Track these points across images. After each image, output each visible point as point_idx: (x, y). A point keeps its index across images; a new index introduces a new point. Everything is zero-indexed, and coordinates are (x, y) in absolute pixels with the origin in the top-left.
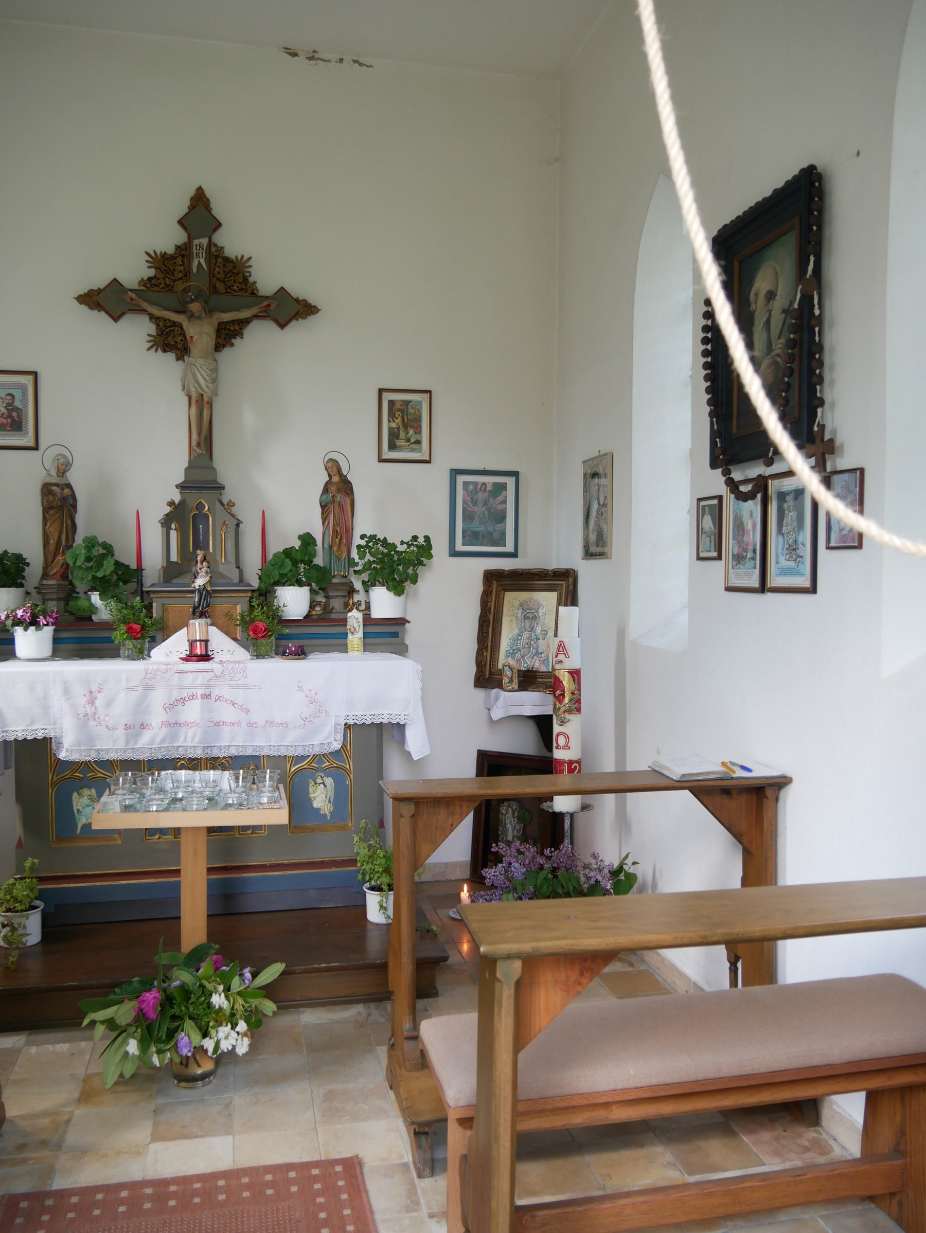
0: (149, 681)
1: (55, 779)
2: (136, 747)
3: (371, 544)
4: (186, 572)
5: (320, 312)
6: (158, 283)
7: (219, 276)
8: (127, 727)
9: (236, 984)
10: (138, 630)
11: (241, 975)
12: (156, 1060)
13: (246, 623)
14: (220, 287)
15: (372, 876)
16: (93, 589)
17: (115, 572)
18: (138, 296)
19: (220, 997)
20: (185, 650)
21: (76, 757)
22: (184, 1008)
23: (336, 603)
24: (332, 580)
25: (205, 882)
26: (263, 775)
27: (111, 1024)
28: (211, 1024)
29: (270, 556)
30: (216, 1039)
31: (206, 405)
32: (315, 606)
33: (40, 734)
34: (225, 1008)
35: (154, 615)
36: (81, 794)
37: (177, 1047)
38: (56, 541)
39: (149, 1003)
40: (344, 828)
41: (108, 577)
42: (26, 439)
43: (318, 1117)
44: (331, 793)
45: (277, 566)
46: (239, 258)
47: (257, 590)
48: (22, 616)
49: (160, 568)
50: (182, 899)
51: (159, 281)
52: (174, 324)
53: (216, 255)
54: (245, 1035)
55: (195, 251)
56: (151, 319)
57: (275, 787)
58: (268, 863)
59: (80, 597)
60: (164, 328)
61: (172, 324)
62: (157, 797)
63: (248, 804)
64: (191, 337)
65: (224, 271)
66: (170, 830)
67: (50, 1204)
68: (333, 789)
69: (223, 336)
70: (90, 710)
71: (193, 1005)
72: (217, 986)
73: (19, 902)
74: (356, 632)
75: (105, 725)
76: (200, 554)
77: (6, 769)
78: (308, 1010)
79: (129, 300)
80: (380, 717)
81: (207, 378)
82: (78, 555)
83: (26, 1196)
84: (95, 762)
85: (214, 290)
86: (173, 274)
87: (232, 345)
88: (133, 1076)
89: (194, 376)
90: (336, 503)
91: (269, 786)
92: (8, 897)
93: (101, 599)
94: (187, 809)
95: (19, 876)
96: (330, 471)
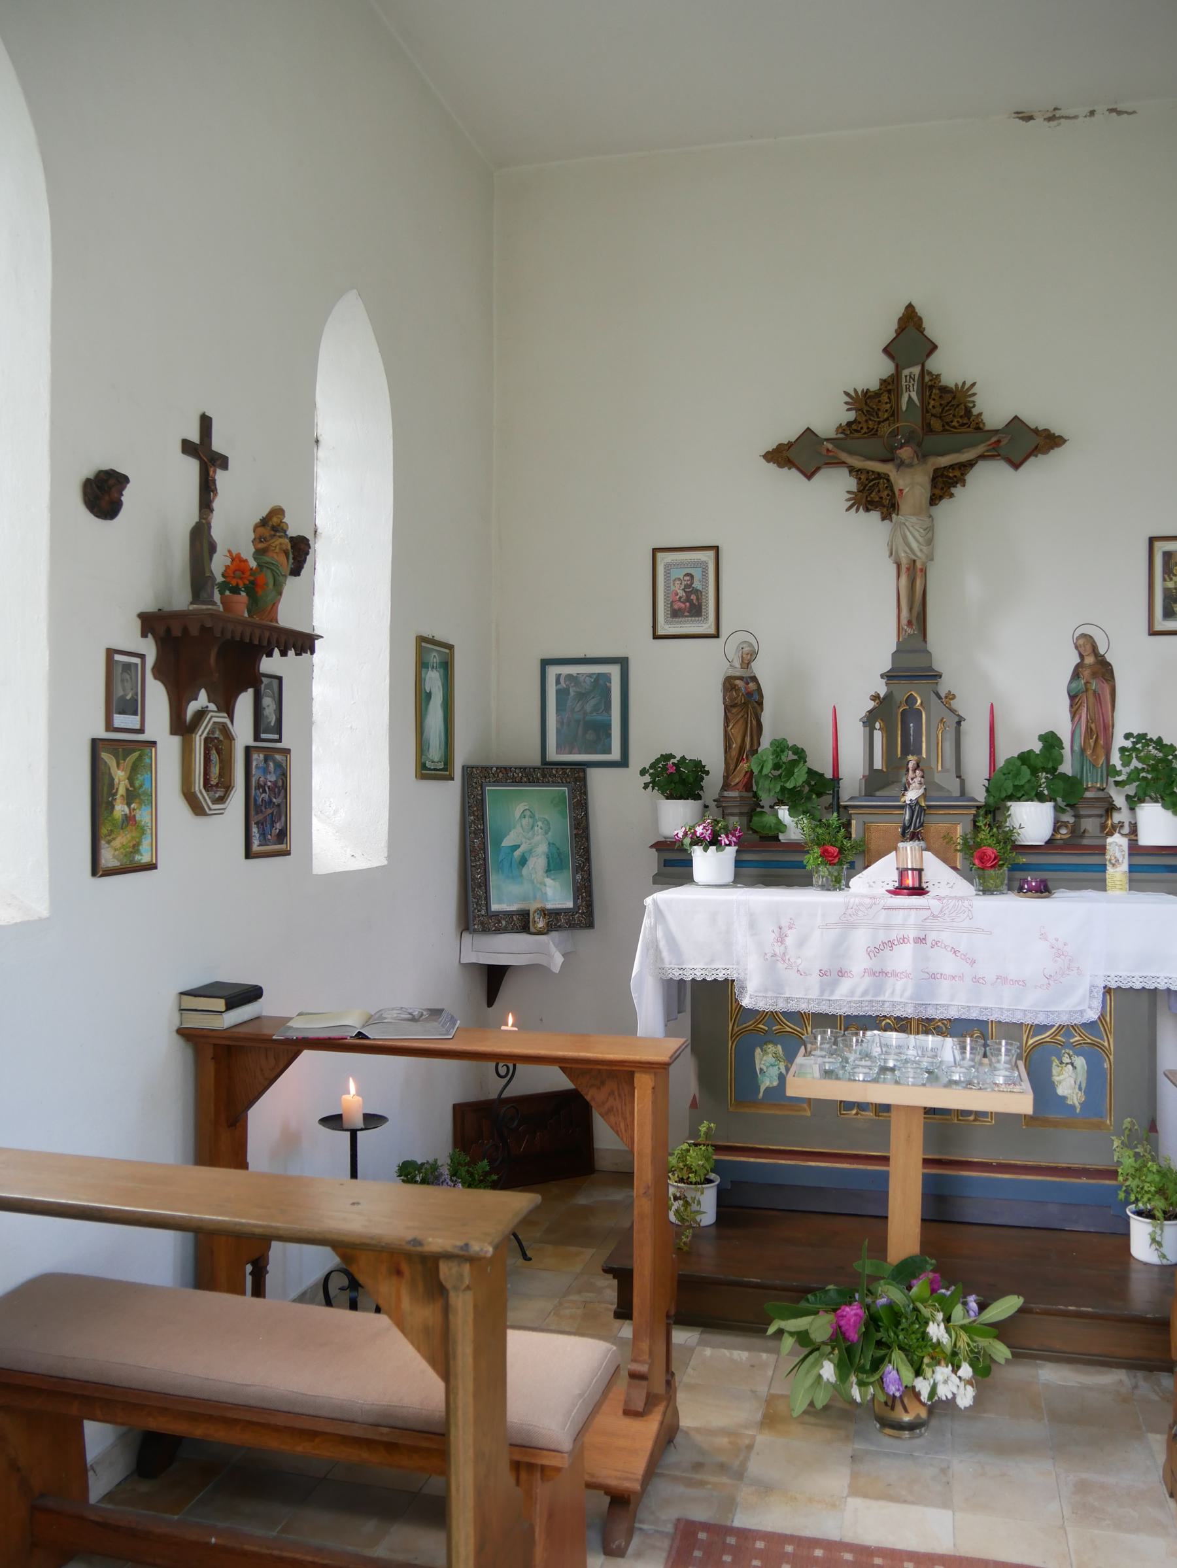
0: (850, 918)
1: (736, 1029)
2: (833, 998)
3: (1139, 746)
4: (893, 782)
5: (1067, 443)
6: (859, 429)
7: (934, 411)
8: (823, 973)
9: (958, 1312)
10: (835, 854)
11: (965, 1304)
12: (856, 1393)
13: (970, 848)
14: (936, 424)
15: (1139, 1196)
16: (781, 802)
17: (807, 782)
18: (836, 446)
19: (939, 1328)
20: (892, 880)
21: (761, 1005)
22: (892, 1334)
23: (1090, 825)
24: (1084, 794)
25: (920, 1177)
26: (996, 1046)
27: (803, 1338)
28: (926, 1360)
29: (1001, 762)
30: (932, 1381)
31: (919, 573)
32: (1059, 828)
33: (721, 975)
34: (945, 1343)
35: (854, 836)
36: (765, 1051)
37: (883, 1382)
38: (739, 745)
39: (849, 1320)
40: (1099, 1126)
41: (799, 789)
42: (706, 626)
43: (1067, 1513)
44: (1082, 1078)
45: (1010, 776)
46: (960, 385)
47: (985, 806)
48: (702, 834)
49: (862, 777)
50: (890, 1195)
51: (860, 426)
52: (879, 476)
53: (930, 385)
54: (969, 1382)
55: (904, 383)
56: (850, 472)
57: (1013, 1064)
58: (994, 1162)
59: (765, 812)
60: (867, 482)
61: (876, 476)
62: (863, 1063)
63: (979, 1083)
64: (901, 490)
65: (941, 405)
66: (870, 1106)
67: (732, 1543)
68: (1086, 1072)
69: (940, 485)
70: (779, 949)
71: (903, 1332)
72: (936, 1313)
73: (693, 1172)
74: (1119, 863)
75: (795, 969)
76: (912, 760)
77: (679, 1012)
78: (1050, 1365)
79: (824, 452)
80: (1154, 980)
81: (921, 539)
82: (765, 761)
83: (706, 1527)
84: (784, 1013)
85: (928, 429)
86: (877, 414)
87: (952, 495)
88: (826, 1408)
89: (905, 538)
90: (1090, 693)
91: (1005, 1063)
92: (681, 1165)
93: (790, 815)
94: (902, 1082)
95: (693, 1141)
96: (1081, 650)
